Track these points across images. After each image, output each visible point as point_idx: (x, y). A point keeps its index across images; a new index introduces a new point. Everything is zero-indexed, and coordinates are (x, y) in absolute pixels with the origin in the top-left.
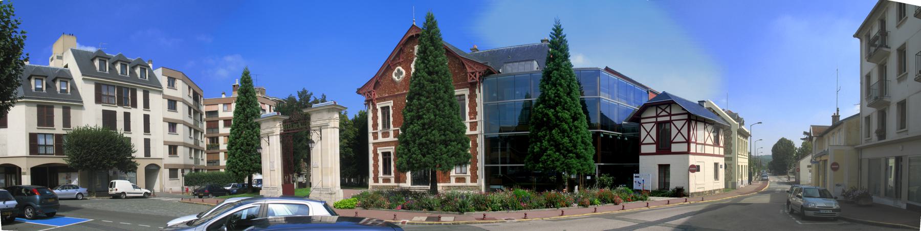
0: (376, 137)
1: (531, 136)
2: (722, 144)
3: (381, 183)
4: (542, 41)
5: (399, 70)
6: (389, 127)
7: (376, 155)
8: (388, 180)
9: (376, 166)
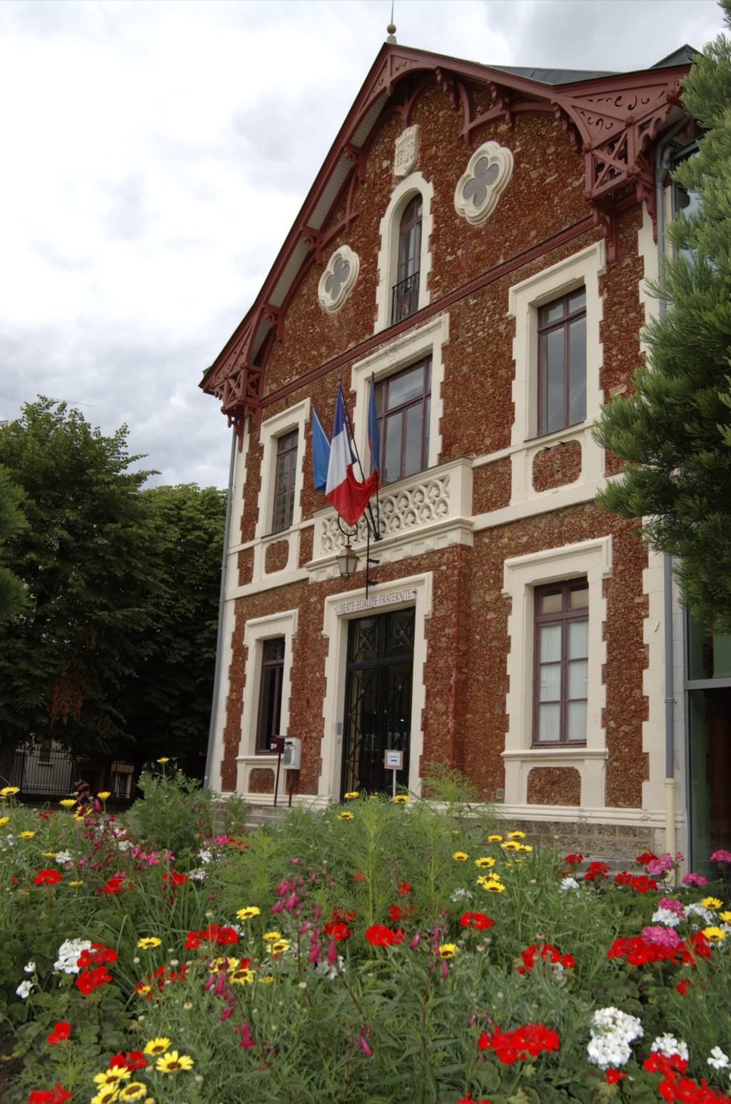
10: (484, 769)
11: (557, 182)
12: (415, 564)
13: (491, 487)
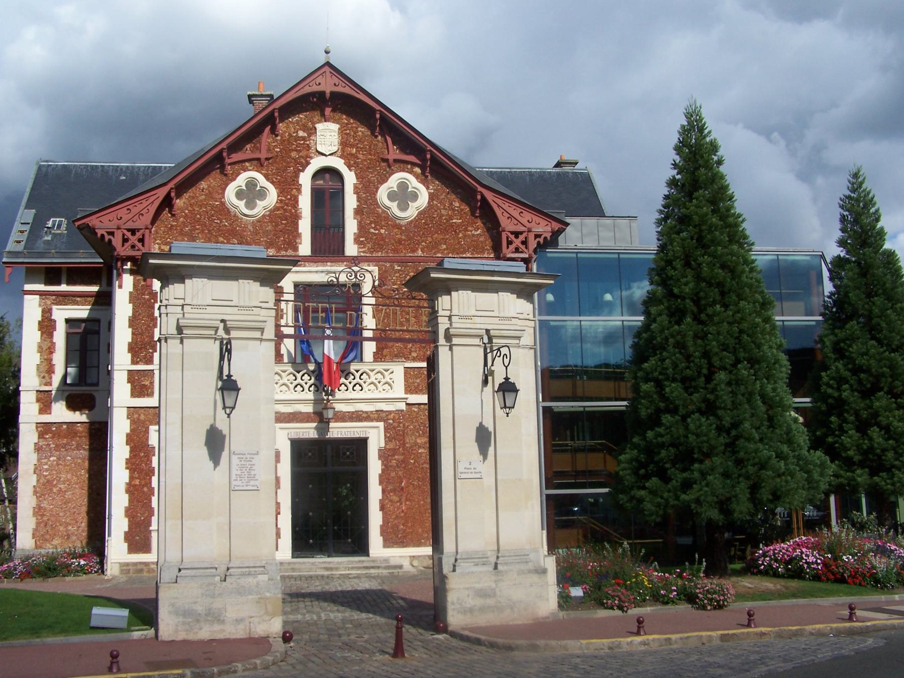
10: (420, 530)
11: (458, 225)
12: (365, 415)
13: (418, 381)
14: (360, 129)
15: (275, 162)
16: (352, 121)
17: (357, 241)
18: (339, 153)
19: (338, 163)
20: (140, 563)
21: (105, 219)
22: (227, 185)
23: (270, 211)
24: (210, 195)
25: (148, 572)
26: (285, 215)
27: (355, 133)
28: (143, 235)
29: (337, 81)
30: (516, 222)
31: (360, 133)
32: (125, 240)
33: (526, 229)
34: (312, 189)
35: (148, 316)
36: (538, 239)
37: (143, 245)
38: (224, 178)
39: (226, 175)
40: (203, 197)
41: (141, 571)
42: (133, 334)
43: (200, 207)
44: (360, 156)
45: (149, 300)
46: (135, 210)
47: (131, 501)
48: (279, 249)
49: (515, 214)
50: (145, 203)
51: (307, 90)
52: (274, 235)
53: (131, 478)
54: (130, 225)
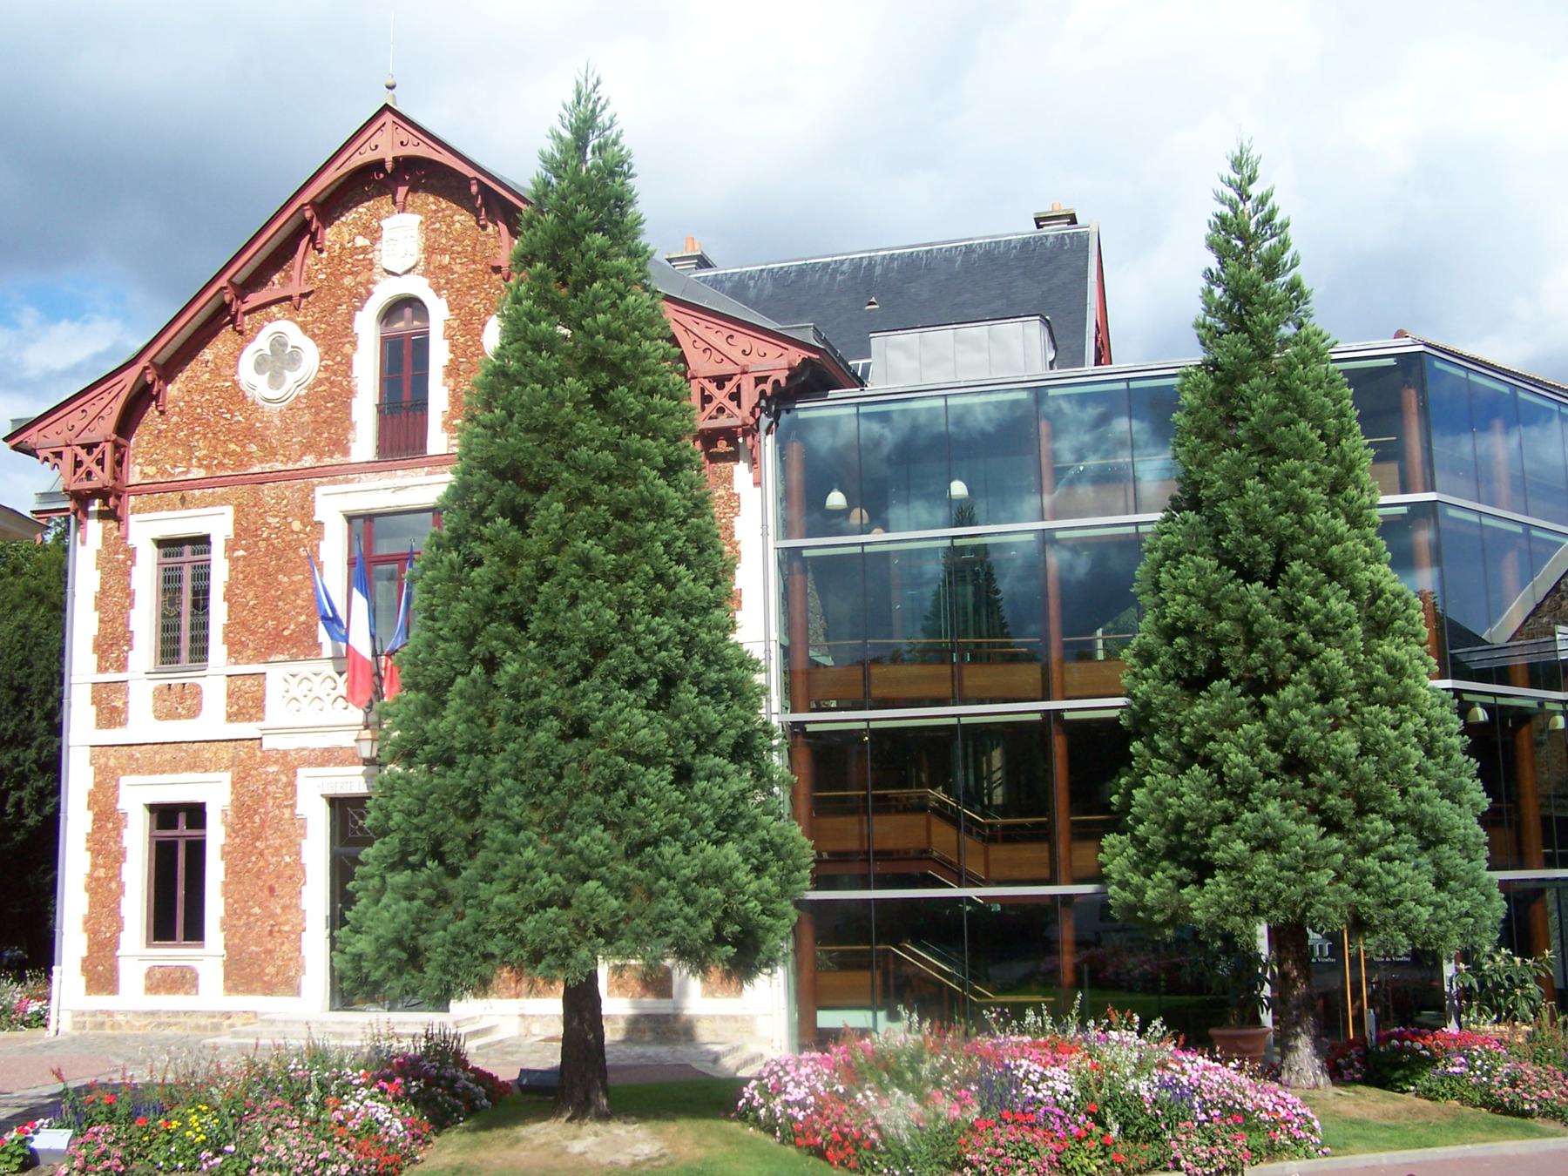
0: (110, 712)
1: (1142, 721)
2: (439, 440)
3: (132, 994)
4: (1039, 222)
5: (279, 343)
6: (200, 652)
7: (106, 816)
8: (181, 981)
9: (105, 893)
14: (456, 218)
15: (318, 299)
16: (444, 205)
17: (447, 426)
18: (421, 268)
19: (418, 286)
20: (101, 1012)
21: (50, 431)
22: (241, 350)
23: (309, 388)
24: (216, 373)
25: (112, 1027)
26: (332, 397)
27: (449, 226)
28: (739, 387)
29: (404, 136)
30: (719, 357)
31: (458, 225)
32: (706, 399)
33: (737, 369)
34: (384, 340)
35: (123, 591)
36: (762, 387)
37: (739, 406)
38: (239, 339)
39: (241, 333)
40: (207, 376)
41: (102, 1025)
42: (101, 621)
43: (202, 393)
44: (457, 268)
45: (124, 562)
46: (92, 411)
47: (92, 905)
48: (320, 455)
49: (718, 341)
50: (107, 397)
51: (358, 161)
52: (314, 430)
53: (95, 866)
54: (87, 437)
